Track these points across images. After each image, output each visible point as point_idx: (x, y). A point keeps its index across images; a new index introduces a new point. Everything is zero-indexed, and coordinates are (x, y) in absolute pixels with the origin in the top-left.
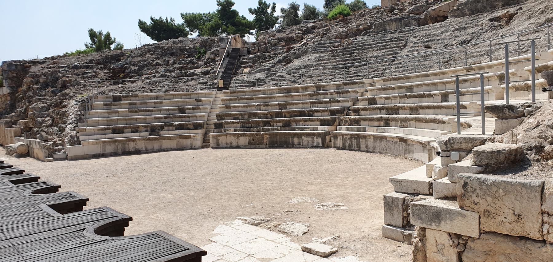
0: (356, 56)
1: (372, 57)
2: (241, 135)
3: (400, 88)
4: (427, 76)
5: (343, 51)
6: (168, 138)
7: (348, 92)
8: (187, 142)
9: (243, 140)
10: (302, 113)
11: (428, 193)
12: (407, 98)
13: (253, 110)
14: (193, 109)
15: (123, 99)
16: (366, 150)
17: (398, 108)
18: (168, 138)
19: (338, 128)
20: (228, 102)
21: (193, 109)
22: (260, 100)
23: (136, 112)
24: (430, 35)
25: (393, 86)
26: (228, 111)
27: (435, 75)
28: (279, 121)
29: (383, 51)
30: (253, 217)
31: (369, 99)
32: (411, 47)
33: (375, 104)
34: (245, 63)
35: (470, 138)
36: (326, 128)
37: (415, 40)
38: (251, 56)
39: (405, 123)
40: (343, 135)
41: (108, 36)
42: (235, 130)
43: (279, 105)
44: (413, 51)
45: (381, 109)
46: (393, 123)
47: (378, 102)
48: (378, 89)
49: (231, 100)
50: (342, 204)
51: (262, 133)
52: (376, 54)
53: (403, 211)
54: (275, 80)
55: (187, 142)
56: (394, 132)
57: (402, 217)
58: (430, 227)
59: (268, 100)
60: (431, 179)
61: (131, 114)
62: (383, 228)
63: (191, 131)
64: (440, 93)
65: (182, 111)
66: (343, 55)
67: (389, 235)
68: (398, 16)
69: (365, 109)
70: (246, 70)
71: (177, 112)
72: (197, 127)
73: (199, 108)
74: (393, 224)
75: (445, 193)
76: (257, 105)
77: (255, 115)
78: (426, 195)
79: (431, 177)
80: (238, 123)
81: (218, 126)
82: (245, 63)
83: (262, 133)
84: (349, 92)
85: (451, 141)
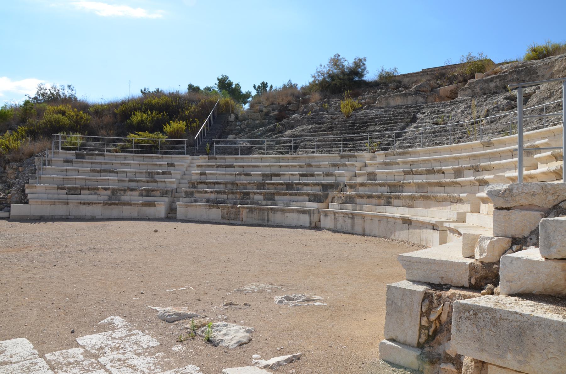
3: (405, 163)
5: (342, 124)
6: (129, 204)
8: (150, 211)
9: (215, 213)
10: (289, 186)
11: (467, 285)
13: (230, 179)
14: (163, 173)
15: (87, 157)
16: (361, 232)
17: (402, 185)
18: (129, 204)
19: (330, 204)
20: (204, 169)
21: (163, 173)
23: (98, 172)
24: (438, 111)
26: (203, 178)
28: (261, 194)
29: (386, 126)
30: (166, 309)
31: (369, 174)
32: (418, 123)
33: (375, 180)
36: (314, 205)
37: (422, 116)
39: (411, 202)
40: (335, 213)
41: (263, 83)
43: (263, 175)
44: (420, 127)
45: (381, 185)
46: (394, 201)
47: (378, 178)
48: (380, 164)
49: (209, 166)
50: (317, 297)
52: (378, 129)
53: (422, 315)
55: (150, 211)
56: (396, 212)
57: (418, 327)
58: (500, 363)
59: (250, 169)
60: (472, 261)
61: (91, 174)
62: (382, 345)
63: (157, 199)
64: (453, 169)
65: (150, 174)
66: (342, 127)
67: (391, 359)
68: (404, 92)
69: (363, 185)
71: (144, 175)
72: (164, 193)
73: (170, 173)
74: (401, 338)
75: (528, 285)
76: (238, 174)
77: (234, 184)
78: (462, 288)
79: (472, 257)
80: (212, 192)
81: (189, 194)
84: (346, 165)
85: (515, 191)
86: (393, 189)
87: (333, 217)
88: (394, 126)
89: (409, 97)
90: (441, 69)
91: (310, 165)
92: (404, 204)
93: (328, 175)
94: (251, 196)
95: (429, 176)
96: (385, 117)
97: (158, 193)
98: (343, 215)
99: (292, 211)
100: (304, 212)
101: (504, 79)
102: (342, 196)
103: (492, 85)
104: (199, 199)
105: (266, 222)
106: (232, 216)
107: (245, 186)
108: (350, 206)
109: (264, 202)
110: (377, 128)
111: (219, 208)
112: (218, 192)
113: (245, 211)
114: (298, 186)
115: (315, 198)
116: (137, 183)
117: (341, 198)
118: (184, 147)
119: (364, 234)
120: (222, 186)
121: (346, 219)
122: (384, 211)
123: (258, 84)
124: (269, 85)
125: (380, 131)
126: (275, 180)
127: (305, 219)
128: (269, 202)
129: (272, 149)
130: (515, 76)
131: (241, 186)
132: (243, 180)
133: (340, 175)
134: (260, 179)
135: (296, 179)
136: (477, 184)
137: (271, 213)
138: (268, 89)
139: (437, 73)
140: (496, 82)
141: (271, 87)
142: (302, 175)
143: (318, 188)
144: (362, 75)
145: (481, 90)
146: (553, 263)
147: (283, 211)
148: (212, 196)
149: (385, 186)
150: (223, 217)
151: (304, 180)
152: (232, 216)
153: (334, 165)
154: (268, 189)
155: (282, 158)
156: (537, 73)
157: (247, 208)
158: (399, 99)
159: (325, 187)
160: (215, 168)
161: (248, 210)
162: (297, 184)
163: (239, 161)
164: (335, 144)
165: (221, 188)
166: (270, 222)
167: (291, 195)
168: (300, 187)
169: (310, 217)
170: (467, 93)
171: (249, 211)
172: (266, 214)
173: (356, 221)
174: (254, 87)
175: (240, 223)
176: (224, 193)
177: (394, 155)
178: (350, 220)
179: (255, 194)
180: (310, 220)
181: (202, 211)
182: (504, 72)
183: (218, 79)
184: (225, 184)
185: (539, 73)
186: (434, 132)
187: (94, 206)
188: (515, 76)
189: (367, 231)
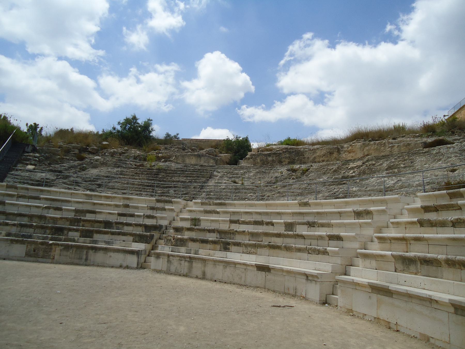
0: (161, 178)
1: (178, 181)
2: (17, 242)
4: (101, 197)
5: (147, 171)
7: (164, 209)
9: (19, 250)
10: (108, 224)
12: (239, 224)
22: (49, 202)
25: (218, 210)
27: (107, 197)
28: (77, 230)
34: (29, 160)
35: (419, 257)
38: (37, 155)
41: (35, 124)
42: (9, 234)
43: (76, 211)
51: (51, 242)
54: (67, 184)
61: (8, 189)
70: (30, 167)
76: (46, 208)
77: (41, 217)
82: (29, 160)
83: (51, 242)
87: (166, 260)
88: (196, 179)
90: (198, 141)
91: (127, 206)
92: (245, 251)
93: (149, 217)
95: (256, 226)
96: (186, 171)
98: (178, 258)
99: (118, 251)
100: (132, 252)
101: (279, 156)
102: (172, 239)
103: (270, 159)
105: (83, 261)
107: (55, 220)
108: (183, 249)
109: (82, 239)
110: (182, 179)
111: (24, 244)
112: (22, 226)
113: (58, 249)
114: (117, 225)
115: (140, 239)
117: (170, 240)
120: (26, 219)
121: (183, 262)
122: (225, 256)
123: (31, 123)
124: (40, 126)
125: (185, 182)
126: (89, 217)
127: (132, 260)
129: (79, 186)
130: (288, 155)
131: (51, 221)
132: (52, 214)
133: (162, 218)
134: (71, 215)
135: (113, 219)
136: (328, 239)
137: (91, 252)
138: (38, 130)
139: (214, 144)
140: (273, 157)
141: (42, 128)
142: (232, 222)
144: (150, 132)
145: (261, 161)
146: (325, 297)
147: (106, 250)
148: (14, 230)
149: (214, 232)
151: (235, 227)
153: (152, 208)
154: (83, 226)
156: (304, 155)
157: (62, 245)
158: (194, 158)
159: (147, 228)
160: (15, 198)
161: (62, 247)
162: (117, 223)
164: (144, 189)
165: (25, 221)
166: (88, 261)
167: (113, 234)
168: (120, 226)
169: (138, 258)
170: (249, 161)
171: (64, 249)
172: (85, 252)
173: (194, 264)
174: (27, 125)
176: (31, 226)
177: (210, 205)
178: (187, 264)
179: (70, 230)
180: (138, 261)
182: (277, 151)
184: (31, 217)
186: (235, 189)
188: (288, 155)
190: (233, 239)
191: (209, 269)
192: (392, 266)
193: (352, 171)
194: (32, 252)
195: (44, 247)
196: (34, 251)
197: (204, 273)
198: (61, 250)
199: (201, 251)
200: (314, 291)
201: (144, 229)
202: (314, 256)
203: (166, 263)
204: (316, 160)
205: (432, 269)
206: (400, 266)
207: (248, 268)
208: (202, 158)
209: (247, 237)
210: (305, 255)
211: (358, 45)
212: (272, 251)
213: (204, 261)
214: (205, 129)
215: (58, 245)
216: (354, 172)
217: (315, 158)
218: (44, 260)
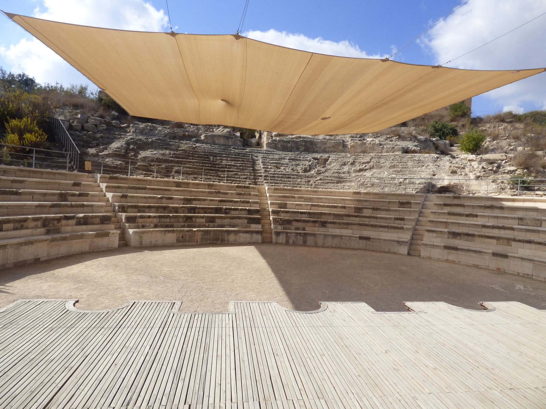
9: (171, 238)
55: (103, 242)
86: (312, 216)
89: (230, 140)
94: (194, 219)
97: (98, 220)
103: (289, 145)
104: (148, 224)
106: (187, 238)
113: (200, 233)
116: (59, 209)
118: (66, 163)
119: (323, 247)
128: (212, 224)
143: (244, 212)
150: (178, 241)
152: (187, 238)
155: (70, 174)
163: (44, 176)
175: (195, 244)
178: (302, 238)
181: (154, 234)
183: (10, 73)
185: (318, 146)
187: (38, 245)
189: (392, 251)
190: (320, 218)
191: (320, 241)
192: (446, 236)
193: (364, 166)
194: (181, 239)
195: (189, 233)
196: (183, 237)
197: (316, 243)
198: (202, 235)
199: (307, 228)
200: (404, 250)
201: (247, 212)
202: (397, 230)
203: (285, 238)
204: (327, 150)
205: (470, 238)
206: (451, 236)
207: (352, 238)
208: (230, 140)
209: (332, 217)
210: (386, 229)
211: (294, 35)
212: (360, 227)
213: (314, 235)
214: (15, 45)
215: (200, 231)
216: (366, 166)
217: (325, 148)
218: (191, 243)
